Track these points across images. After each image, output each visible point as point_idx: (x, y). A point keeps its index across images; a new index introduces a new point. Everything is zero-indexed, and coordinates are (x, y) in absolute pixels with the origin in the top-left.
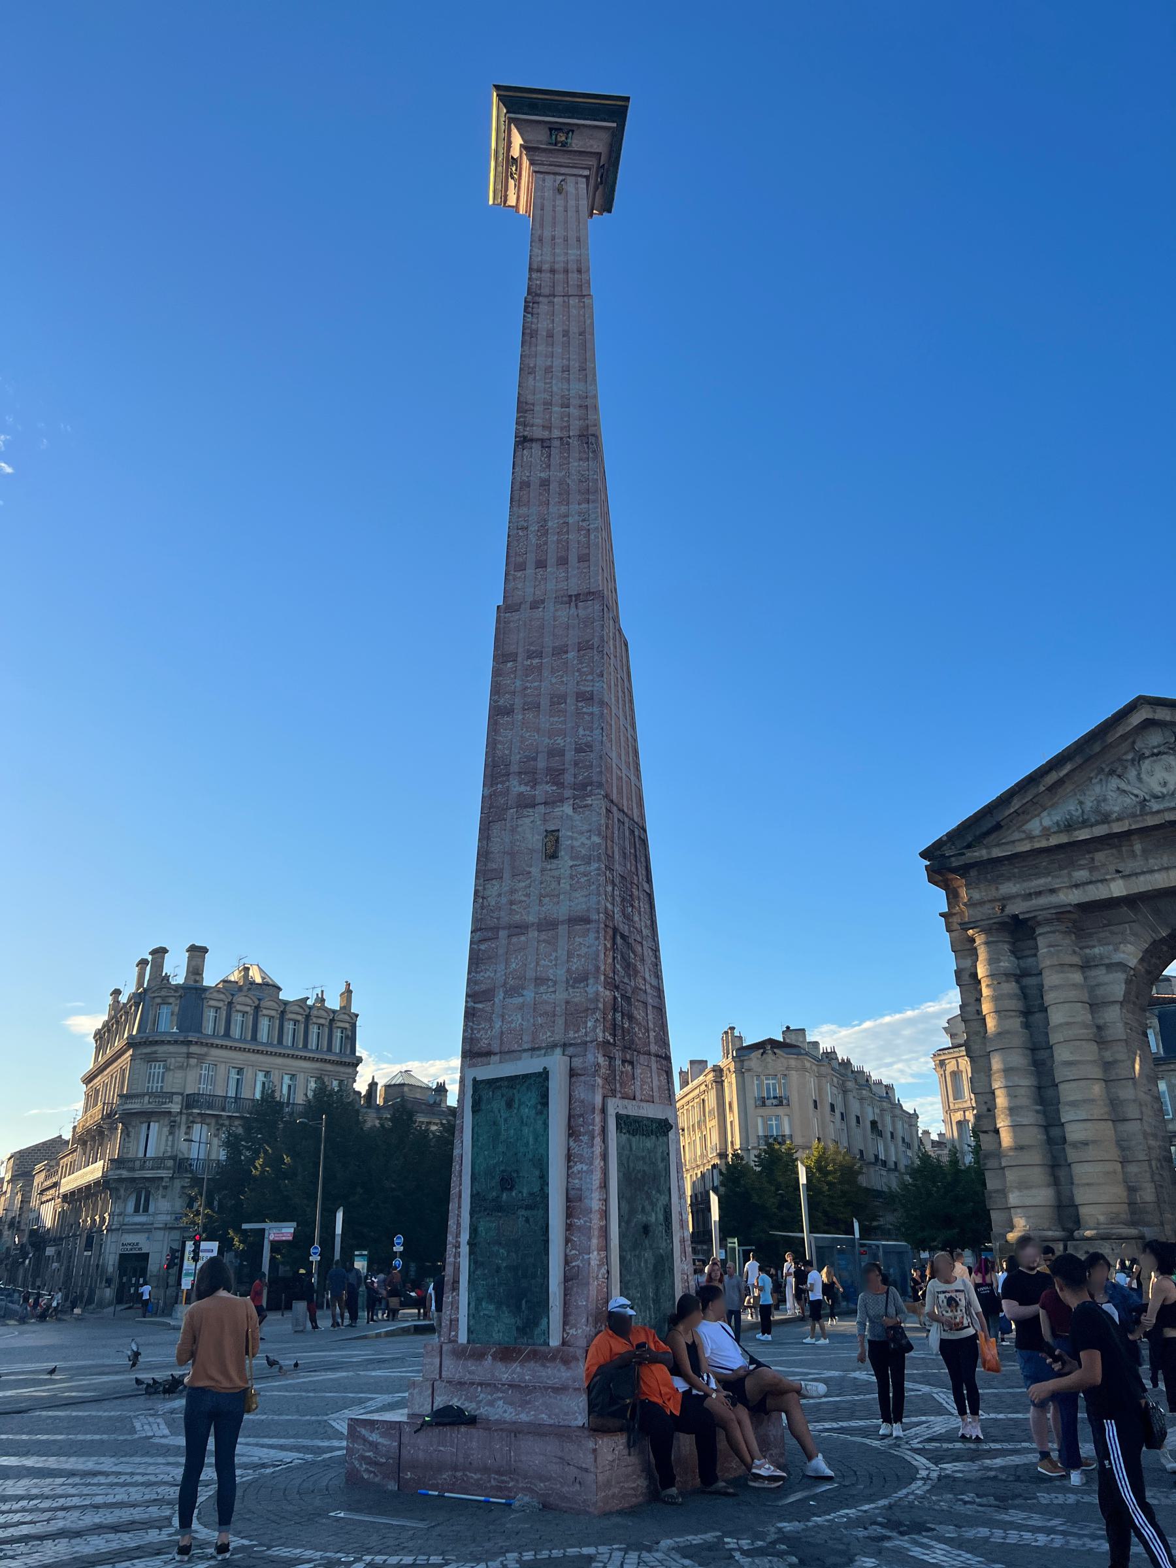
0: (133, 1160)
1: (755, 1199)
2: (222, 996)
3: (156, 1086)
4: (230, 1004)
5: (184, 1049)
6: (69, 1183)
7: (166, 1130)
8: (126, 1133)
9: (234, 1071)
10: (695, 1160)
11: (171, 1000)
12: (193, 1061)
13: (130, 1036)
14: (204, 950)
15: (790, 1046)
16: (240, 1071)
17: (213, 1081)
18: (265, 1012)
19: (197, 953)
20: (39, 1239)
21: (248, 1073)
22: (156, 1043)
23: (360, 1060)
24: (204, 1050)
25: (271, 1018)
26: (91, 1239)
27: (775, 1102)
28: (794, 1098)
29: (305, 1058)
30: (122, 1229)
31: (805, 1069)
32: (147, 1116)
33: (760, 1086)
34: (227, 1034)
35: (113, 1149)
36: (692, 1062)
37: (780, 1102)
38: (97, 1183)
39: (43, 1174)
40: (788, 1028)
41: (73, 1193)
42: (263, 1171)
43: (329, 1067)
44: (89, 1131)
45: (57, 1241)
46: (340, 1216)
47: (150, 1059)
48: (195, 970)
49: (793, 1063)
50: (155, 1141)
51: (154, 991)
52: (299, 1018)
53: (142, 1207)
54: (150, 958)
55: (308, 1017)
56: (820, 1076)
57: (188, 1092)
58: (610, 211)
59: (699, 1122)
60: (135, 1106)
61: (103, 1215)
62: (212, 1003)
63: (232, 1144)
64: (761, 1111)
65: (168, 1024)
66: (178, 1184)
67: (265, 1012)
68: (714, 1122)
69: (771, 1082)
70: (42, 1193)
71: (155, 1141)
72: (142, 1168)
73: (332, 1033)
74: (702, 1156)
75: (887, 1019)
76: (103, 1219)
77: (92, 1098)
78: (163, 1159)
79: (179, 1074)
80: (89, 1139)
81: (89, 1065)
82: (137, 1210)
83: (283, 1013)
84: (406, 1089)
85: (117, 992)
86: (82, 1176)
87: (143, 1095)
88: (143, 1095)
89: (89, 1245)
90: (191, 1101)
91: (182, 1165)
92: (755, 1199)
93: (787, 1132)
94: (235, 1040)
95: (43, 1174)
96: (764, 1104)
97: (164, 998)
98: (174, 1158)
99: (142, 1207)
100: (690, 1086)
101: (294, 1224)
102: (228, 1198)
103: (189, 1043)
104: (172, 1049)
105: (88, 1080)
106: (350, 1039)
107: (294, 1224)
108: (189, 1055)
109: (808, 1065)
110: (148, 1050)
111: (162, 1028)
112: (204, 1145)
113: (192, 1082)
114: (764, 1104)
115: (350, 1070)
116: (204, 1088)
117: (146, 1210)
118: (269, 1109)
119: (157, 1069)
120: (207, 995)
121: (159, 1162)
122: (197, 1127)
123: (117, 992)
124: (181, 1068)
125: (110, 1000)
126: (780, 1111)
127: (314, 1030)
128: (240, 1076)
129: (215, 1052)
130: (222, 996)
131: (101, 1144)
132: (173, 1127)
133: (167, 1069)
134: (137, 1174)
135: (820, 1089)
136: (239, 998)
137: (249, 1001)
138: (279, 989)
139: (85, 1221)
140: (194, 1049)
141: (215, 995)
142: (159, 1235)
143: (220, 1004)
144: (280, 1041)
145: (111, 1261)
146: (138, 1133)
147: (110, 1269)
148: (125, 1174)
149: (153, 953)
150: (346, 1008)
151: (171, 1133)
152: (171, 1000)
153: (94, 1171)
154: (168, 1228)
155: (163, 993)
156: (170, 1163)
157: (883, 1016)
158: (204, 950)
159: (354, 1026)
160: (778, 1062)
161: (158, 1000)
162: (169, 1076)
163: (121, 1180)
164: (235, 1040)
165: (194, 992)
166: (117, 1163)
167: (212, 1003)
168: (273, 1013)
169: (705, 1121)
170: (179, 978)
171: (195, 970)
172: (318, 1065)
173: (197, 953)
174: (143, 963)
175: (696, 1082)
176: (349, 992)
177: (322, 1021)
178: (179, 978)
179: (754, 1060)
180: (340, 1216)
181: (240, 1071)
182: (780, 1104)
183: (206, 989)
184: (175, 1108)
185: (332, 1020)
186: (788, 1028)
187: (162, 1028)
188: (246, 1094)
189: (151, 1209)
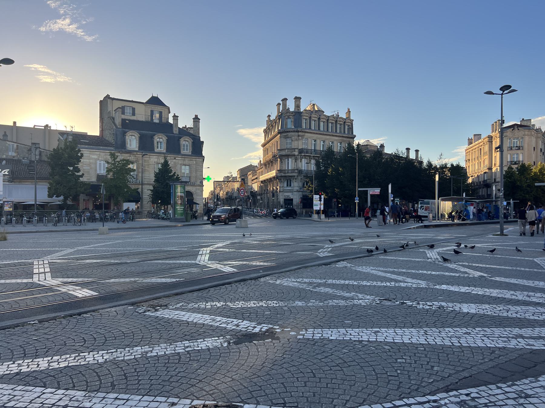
0: (285, 170)
1: (518, 183)
2: (307, 115)
3: (289, 146)
4: (310, 117)
5: (297, 134)
6: (262, 178)
7: (294, 161)
8: (281, 160)
9: (313, 141)
10: (475, 171)
11: (291, 117)
12: (300, 138)
13: (279, 130)
14: (300, 98)
15: (524, 126)
16: (315, 141)
17: (307, 144)
18: (322, 120)
19: (298, 99)
20: (253, 194)
21: (318, 141)
22: (288, 132)
23: (355, 136)
24: (303, 134)
25: (324, 122)
26: (274, 194)
27: (516, 148)
28: (526, 146)
29: (336, 136)
30: (283, 191)
31: (532, 135)
32: (288, 156)
33: (510, 143)
34: (310, 128)
35: (277, 166)
36: (475, 135)
37: (519, 148)
38: (274, 177)
39: (251, 176)
40: (523, 119)
41: (265, 181)
42: (332, 173)
43: (345, 139)
44: (267, 162)
45: (261, 195)
46: (390, 186)
47: (286, 137)
48: (298, 106)
49: (527, 133)
50: (291, 164)
51: (283, 115)
52: (333, 122)
53: (289, 185)
54: (281, 102)
55: (336, 121)
56: (537, 138)
57: (300, 148)
58: (108, 97)
59: (477, 157)
60: (283, 153)
61: (278, 187)
62: (305, 117)
63: (317, 164)
64: (510, 152)
65: (290, 125)
66: (299, 178)
67: (322, 120)
68: (487, 157)
69: (515, 141)
70: (253, 180)
71: (291, 164)
72: (288, 173)
73: (345, 126)
74: (478, 169)
75: (540, 118)
76: (277, 189)
77: (266, 152)
78: (294, 170)
79: (296, 142)
80: (268, 164)
81: (263, 141)
82: (287, 186)
83: (328, 120)
84: (369, 146)
85: (269, 116)
86: (268, 175)
87: (285, 149)
88: (285, 149)
89: (273, 196)
90: (301, 151)
91: (300, 172)
92: (518, 183)
93: (521, 160)
94: (313, 130)
95: (251, 176)
96: (511, 149)
97: (288, 116)
98: (297, 170)
99: (289, 185)
100: (474, 144)
101: (380, 189)
102: (321, 181)
103: (298, 132)
104: (293, 134)
105: (263, 145)
106: (351, 128)
107: (380, 189)
108: (299, 136)
109: (533, 133)
110: (285, 134)
111: (289, 127)
112: (308, 166)
113: (300, 144)
114: (511, 149)
115: (351, 140)
116: (304, 147)
117: (290, 186)
118: (329, 153)
119: (289, 141)
120: (303, 114)
121: (293, 171)
122: (303, 160)
123: (269, 116)
124: (296, 140)
125: (267, 119)
126: (519, 152)
127: (338, 126)
128: (318, 143)
129: (306, 134)
130: (307, 115)
131: (272, 166)
132: (296, 160)
133: (292, 141)
134: (287, 175)
135: (537, 143)
136: (313, 115)
137: (316, 116)
138: (324, 112)
139: (270, 189)
140: (300, 133)
141: (305, 114)
142: (295, 193)
143: (307, 118)
144: (328, 130)
145: (282, 201)
146: (285, 162)
147: (282, 203)
148: (283, 174)
149: (282, 100)
150: (348, 118)
151: (296, 162)
152: (291, 117)
153: (273, 174)
154: (297, 191)
155: (288, 114)
156: (296, 171)
157: (538, 117)
158: (300, 98)
159: (352, 124)
160: (519, 133)
161: (287, 117)
162: (293, 143)
163: (281, 176)
164: (313, 130)
165: (298, 114)
166: (280, 171)
167: (305, 117)
168: (324, 120)
169: (481, 157)
170: (292, 109)
171: (298, 106)
172: (341, 138)
173: (298, 99)
174: (279, 104)
175: (477, 142)
176: (349, 111)
177: (341, 123)
178: (292, 109)
179: (509, 133)
180: (390, 186)
181: (315, 141)
182: (519, 149)
183: (301, 113)
184: (296, 153)
185: (345, 122)
186: (523, 119)
187: (289, 127)
188: (318, 148)
189: (292, 186)
